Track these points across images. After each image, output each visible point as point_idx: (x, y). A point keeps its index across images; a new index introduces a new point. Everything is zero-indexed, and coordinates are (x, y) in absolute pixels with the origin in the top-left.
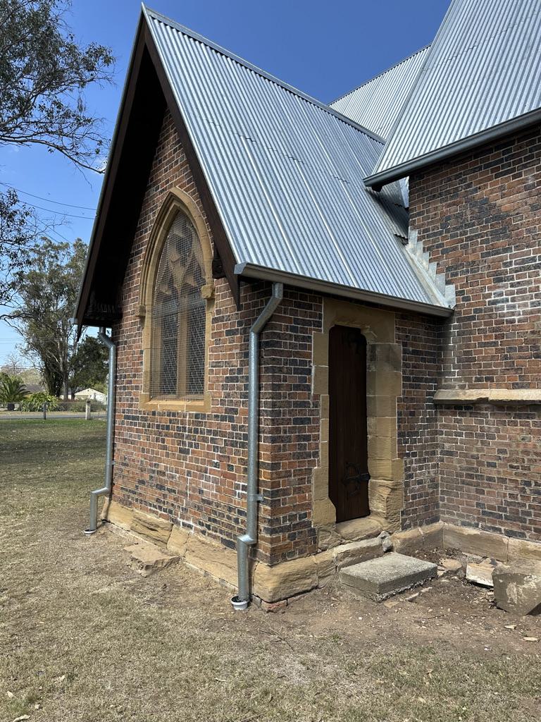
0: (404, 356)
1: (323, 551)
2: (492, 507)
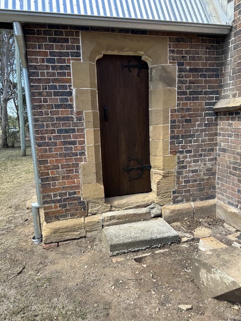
0: (179, 75)
1: (92, 215)
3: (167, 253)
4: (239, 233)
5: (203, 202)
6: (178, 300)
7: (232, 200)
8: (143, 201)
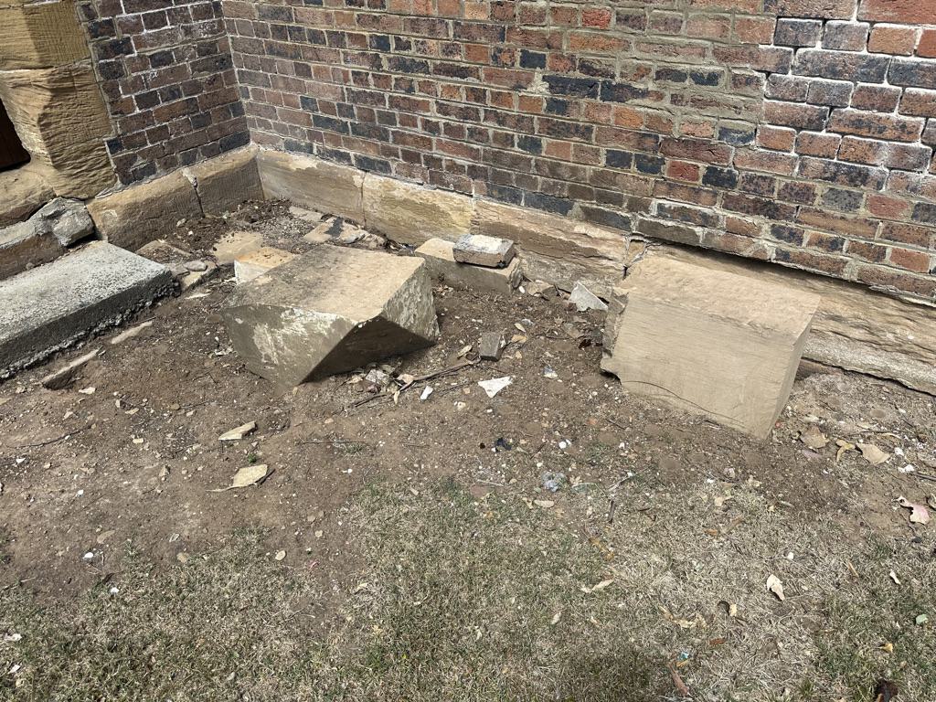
2: (327, 107)
3: (152, 332)
4: (331, 220)
5: (218, 160)
6: (216, 427)
7: (295, 135)
8: (7, 201)
